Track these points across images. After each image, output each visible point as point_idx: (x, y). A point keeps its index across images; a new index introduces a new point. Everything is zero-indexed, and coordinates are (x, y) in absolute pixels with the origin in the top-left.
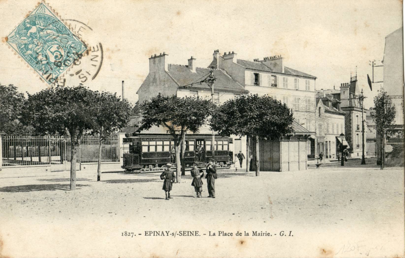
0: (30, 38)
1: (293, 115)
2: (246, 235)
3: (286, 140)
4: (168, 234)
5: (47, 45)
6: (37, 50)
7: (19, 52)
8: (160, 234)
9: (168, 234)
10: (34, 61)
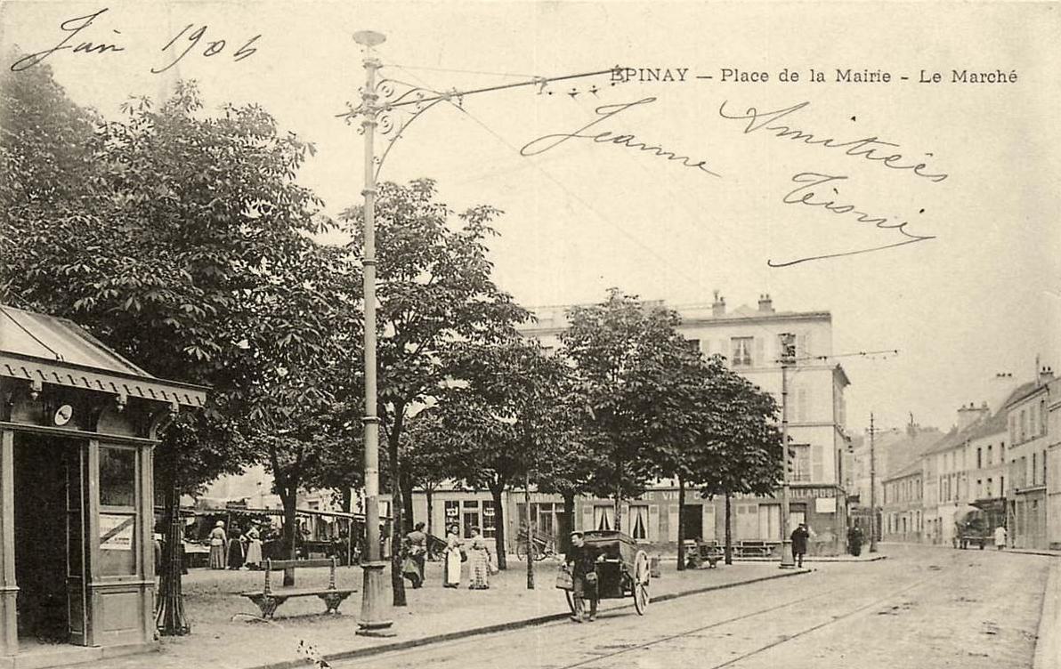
1: (338, 247)
2: (815, 78)
3: (104, 347)
4: (682, 76)
7: (805, 184)
8: (662, 76)
9: (682, 76)
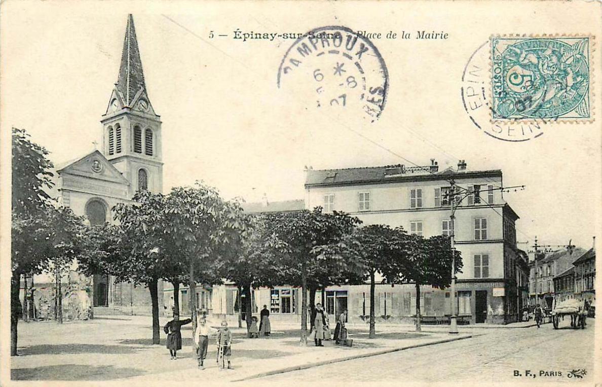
0: (564, 67)
5: (539, 78)
6: (543, 62)
7: (561, 40)
10: (534, 47)
